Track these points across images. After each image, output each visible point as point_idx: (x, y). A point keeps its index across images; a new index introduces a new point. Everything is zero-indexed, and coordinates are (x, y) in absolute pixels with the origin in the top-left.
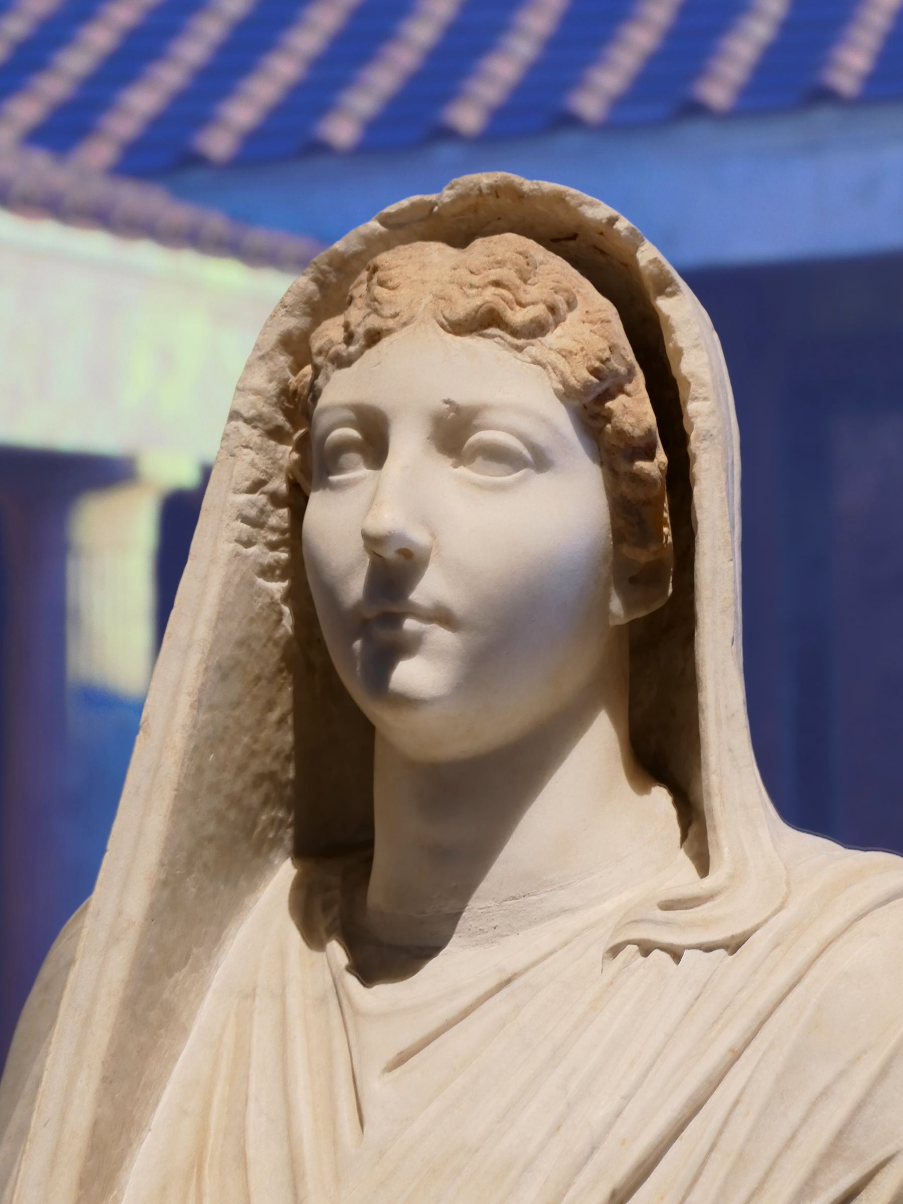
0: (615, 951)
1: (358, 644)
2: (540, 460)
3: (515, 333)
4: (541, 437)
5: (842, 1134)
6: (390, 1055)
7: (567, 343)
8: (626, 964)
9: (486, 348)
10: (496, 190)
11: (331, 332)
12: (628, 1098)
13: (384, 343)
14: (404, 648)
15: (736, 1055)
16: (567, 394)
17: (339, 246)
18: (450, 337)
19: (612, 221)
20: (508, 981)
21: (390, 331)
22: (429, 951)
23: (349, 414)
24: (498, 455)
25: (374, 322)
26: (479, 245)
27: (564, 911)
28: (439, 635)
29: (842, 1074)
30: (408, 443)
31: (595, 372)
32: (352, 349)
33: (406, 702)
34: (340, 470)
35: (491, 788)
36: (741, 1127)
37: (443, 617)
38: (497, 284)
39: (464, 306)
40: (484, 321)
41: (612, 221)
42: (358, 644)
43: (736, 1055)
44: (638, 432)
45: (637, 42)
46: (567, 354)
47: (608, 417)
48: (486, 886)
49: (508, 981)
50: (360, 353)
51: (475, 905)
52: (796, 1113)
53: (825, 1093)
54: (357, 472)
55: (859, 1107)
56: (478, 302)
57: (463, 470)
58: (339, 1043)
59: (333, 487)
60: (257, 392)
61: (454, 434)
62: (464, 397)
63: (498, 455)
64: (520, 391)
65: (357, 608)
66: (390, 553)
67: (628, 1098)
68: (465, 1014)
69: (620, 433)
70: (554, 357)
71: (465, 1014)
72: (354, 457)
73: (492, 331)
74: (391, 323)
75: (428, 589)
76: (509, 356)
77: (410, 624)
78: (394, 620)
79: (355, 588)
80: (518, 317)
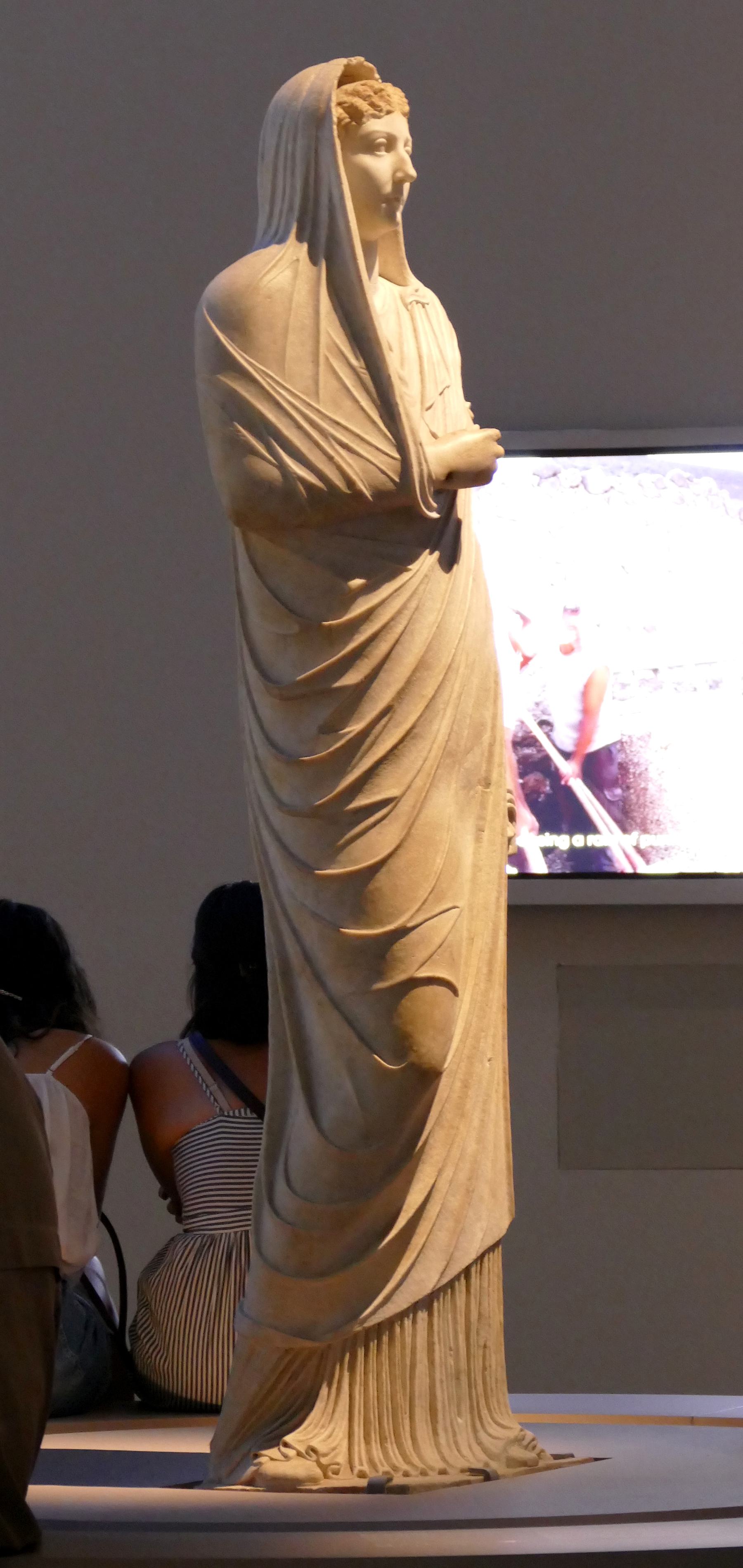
25: (388, 108)
32: (382, 114)
42: (384, 205)
65: (388, 194)
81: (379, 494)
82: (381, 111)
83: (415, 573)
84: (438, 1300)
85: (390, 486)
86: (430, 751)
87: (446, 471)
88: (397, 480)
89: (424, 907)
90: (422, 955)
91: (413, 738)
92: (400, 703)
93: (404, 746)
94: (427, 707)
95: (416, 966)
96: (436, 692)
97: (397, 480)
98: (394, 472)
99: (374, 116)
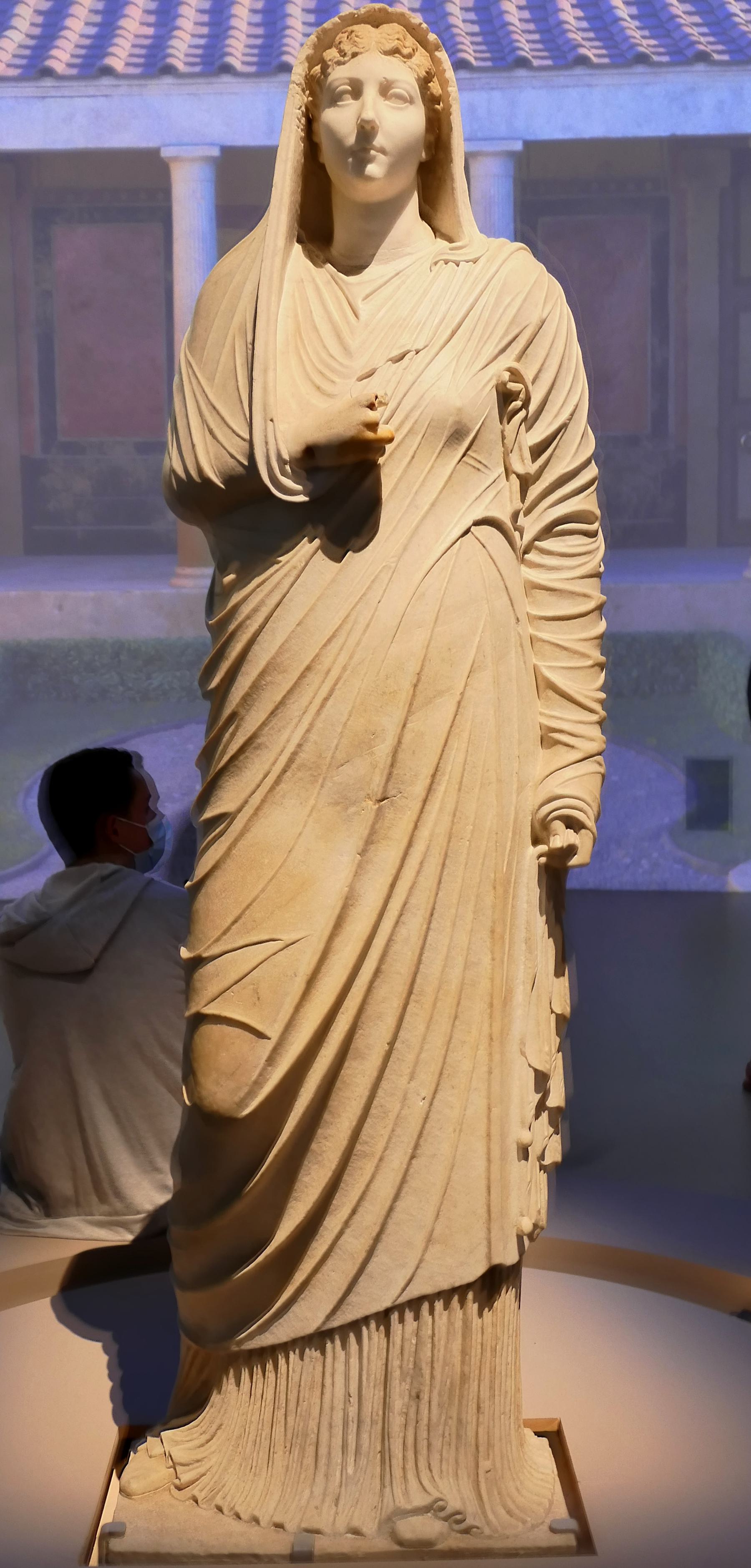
0: (436, 263)
1: (350, 160)
2: (411, 101)
3: (404, 57)
4: (413, 94)
5: (515, 317)
6: (363, 295)
7: (418, 62)
8: (441, 266)
9: (395, 60)
10: (380, 10)
11: (331, 54)
12: (451, 304)
13: (359, 57)
14: (370, 160)
15: (482, 292)
16: (418, 80)
17: (325, 25)
18: (383, 56)
19: (421, 24)
20: (398, 274)
21: (361, 53)
22: (367, 266)
23: (348, 81)
24: (399, 97)
25: (355, 49)
26: (385, 27)
27: (409, 254)
28: (381, 157)
29: (513, 300)
30: (370, 93)
31: (427, 73)
32: (346, 59)
33: (370, 179)
34: (342, 100)
35: (382, 214)
36: (486, 314)
37: (383, 151)
38: (398, 39)
39: (389, 46)
40: (395, 52)
41: (421, 24)
42: (350, 160)
43: (482, 292)
44: (437, 95)
45: (78, 26)
46: (419, 66)
47: (428, 88)
48: (384, 245)
49: (398, 274)
50: (349, 60)
51: (381, 251)
52: (501, 311)
53: (509, 305)
54: (349, 101)
55: (519, 310)
56: (393, 45)
57: (387, 102)
58: (340, 293)
59: (338, 106)
60: (300, 75)
61: (385, 90)
62: (390, 76)
63: (399, 97)
64: (405, 75)
65: (351, 147)
66: (368, 127)
67: (451, 304)
68: (386, 283)
69: (432, 94)
70: (415, 67)
71: (386, 283)
72: (348, 96)
73: (397, 55)
74: (362, 50)
75: (379, 141)
76: (402, 64)
77: (373, 152)
78: (366, 150)
79: (351, 140)
80: (406, 51)
81: (230, 480)
82: (345, 55)
83: (283, 566)
84: (333, 1342)
85: (240, 470)
86: (274, 764)
87: (303, 447)
88: (246, 463)
89: (402, 918)
90: (212, 989)
91: (256, 748)
92: (248, 711)
93: (247, 757)
94: (273, 713)
95: (203, 1003)
96: (285, 697)
97: (246, 463)
98: (243, 454)
99: (339, 63)
